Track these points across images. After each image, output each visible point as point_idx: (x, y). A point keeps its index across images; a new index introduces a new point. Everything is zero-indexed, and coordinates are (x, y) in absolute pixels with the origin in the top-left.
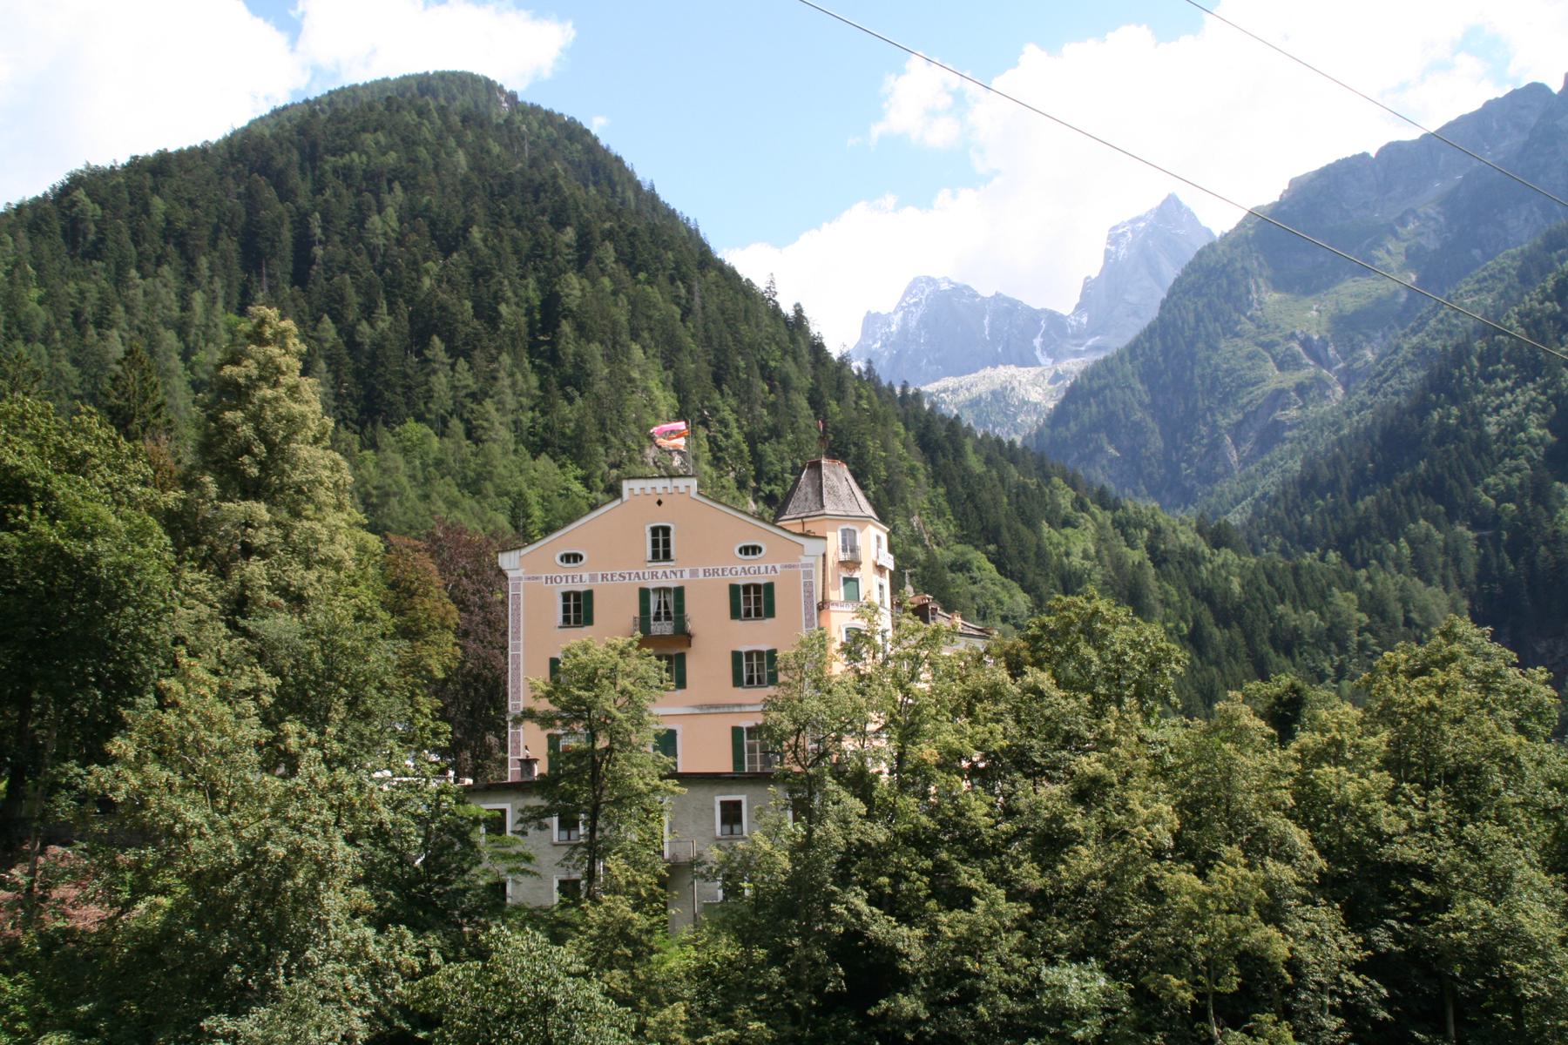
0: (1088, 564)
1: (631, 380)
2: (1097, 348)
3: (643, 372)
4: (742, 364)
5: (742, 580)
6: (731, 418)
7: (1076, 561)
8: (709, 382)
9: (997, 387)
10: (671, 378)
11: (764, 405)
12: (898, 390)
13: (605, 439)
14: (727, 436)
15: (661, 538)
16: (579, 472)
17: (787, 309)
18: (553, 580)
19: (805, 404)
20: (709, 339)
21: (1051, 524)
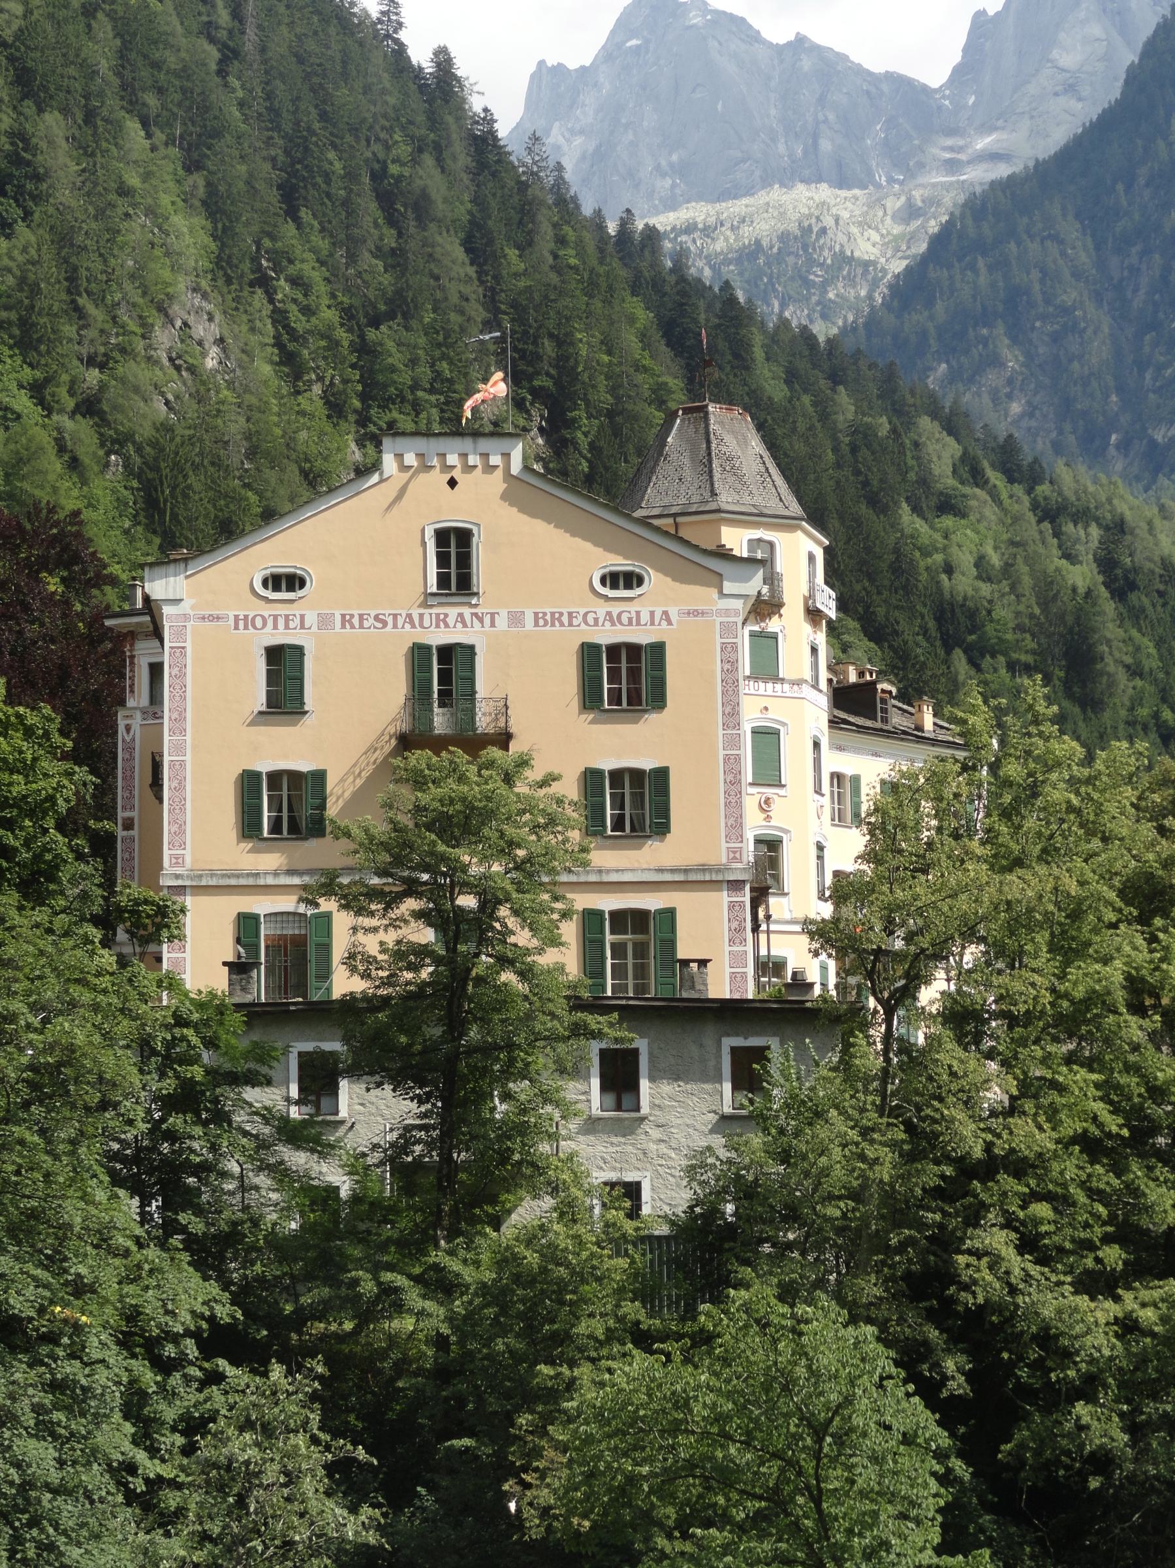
0: (986, 589)
1: (124, 191)
2: (993, 157)
3: (147, 176)
4: (338, 166)
5: (606, 636)
6: (315, 276)
7: (964, 584)
8: (273, 197)
9: (793, 228)
10: (201, 191)
11: (378, 253)
12: (612, 228)
13: (77, 309)
14: (308, 311)
15: (453, 550)
16: (27, 374)
17: (421, 55)
18: (249, 622)
19: (459, 253)
20: (274, 112)
21: (916, 509)
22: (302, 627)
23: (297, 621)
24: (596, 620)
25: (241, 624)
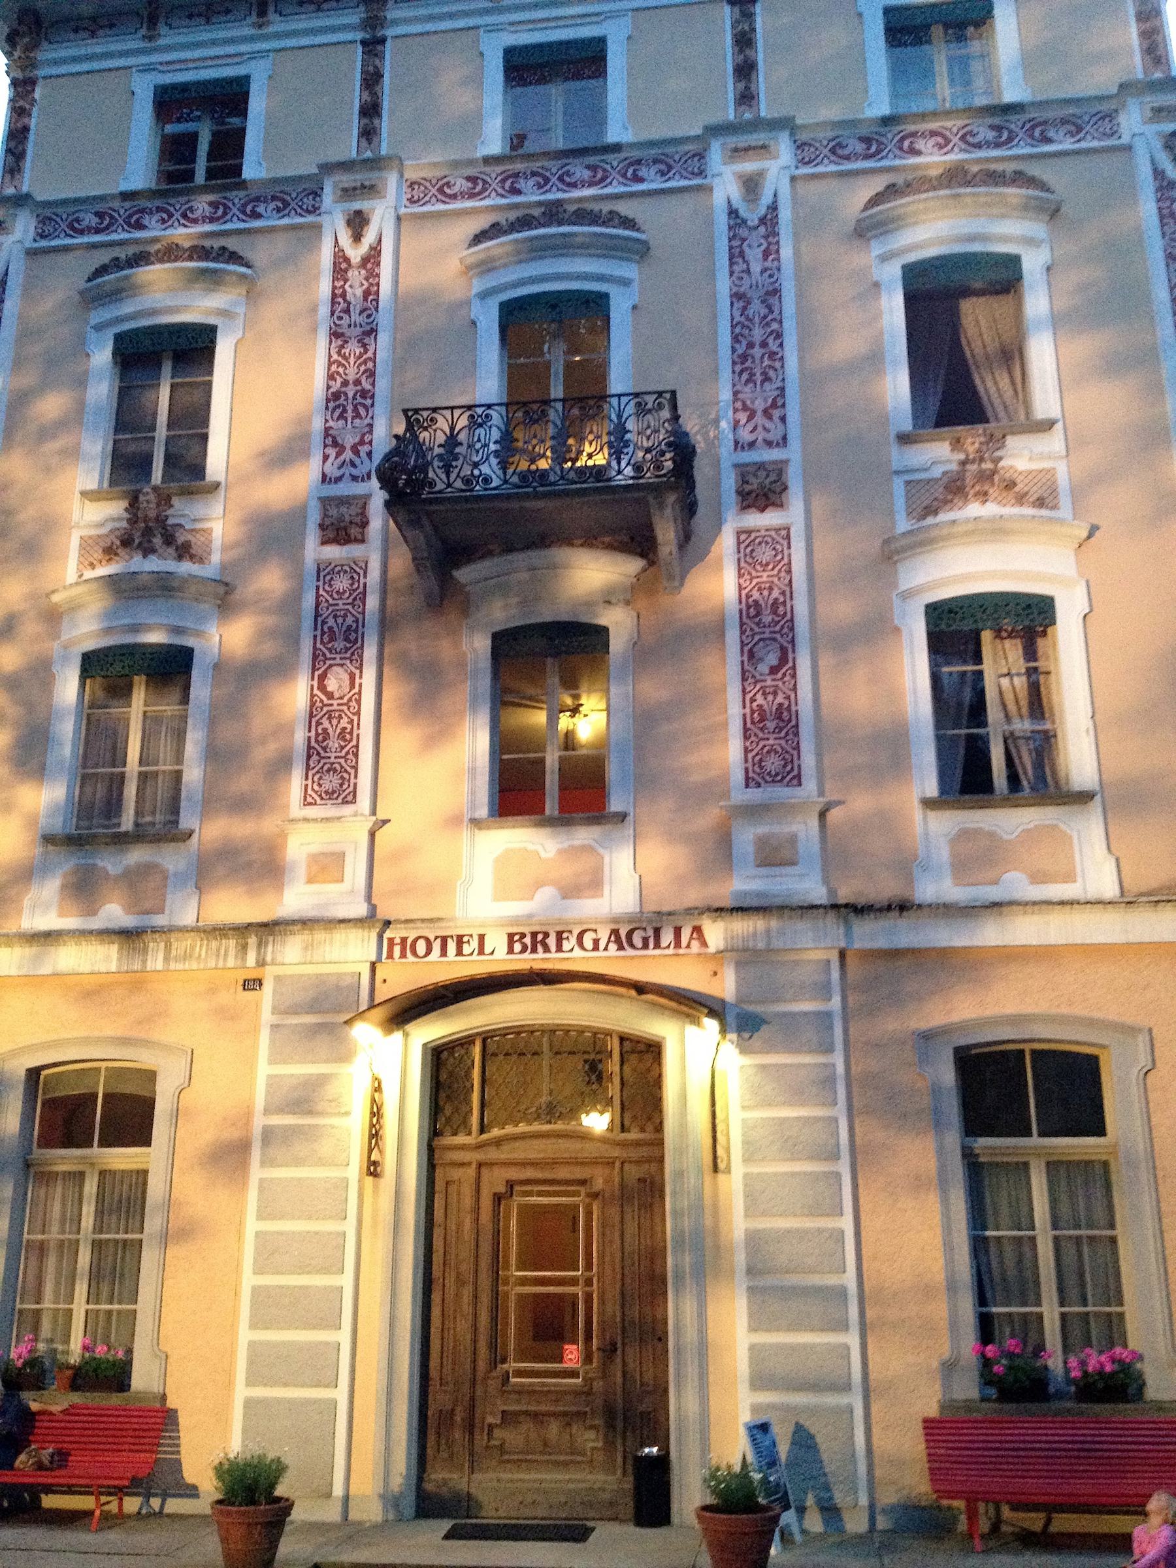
22: (481, 951)
23: (475, 944)
24: (596, 942)
25: (397, 950)
